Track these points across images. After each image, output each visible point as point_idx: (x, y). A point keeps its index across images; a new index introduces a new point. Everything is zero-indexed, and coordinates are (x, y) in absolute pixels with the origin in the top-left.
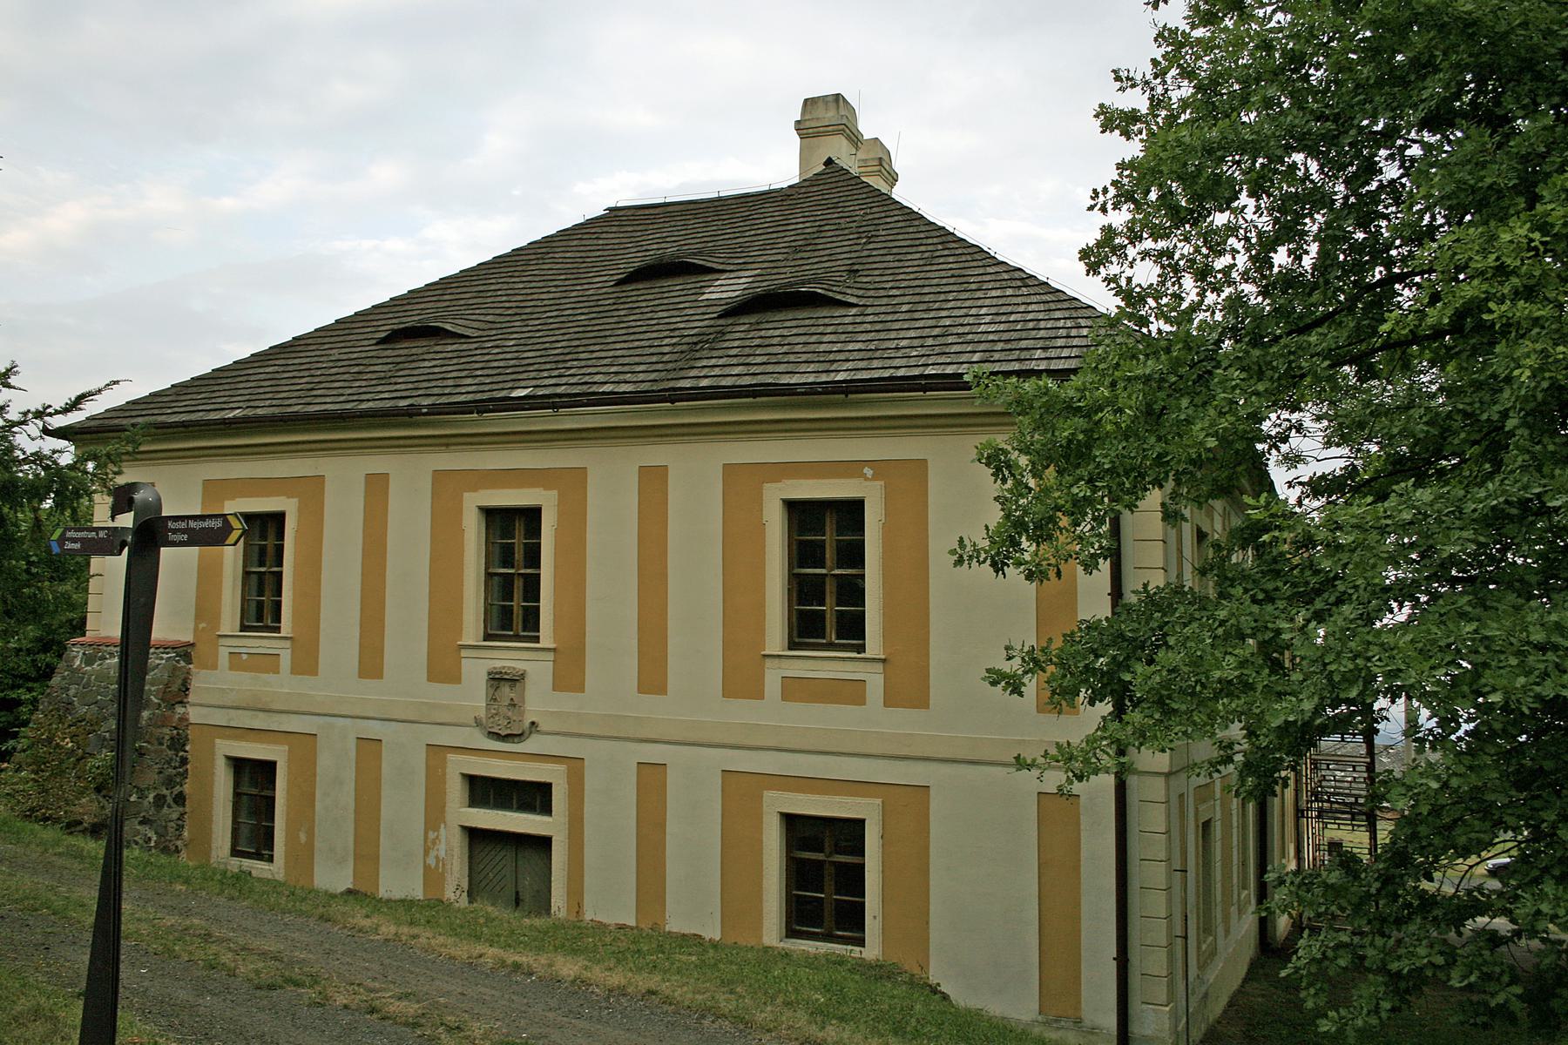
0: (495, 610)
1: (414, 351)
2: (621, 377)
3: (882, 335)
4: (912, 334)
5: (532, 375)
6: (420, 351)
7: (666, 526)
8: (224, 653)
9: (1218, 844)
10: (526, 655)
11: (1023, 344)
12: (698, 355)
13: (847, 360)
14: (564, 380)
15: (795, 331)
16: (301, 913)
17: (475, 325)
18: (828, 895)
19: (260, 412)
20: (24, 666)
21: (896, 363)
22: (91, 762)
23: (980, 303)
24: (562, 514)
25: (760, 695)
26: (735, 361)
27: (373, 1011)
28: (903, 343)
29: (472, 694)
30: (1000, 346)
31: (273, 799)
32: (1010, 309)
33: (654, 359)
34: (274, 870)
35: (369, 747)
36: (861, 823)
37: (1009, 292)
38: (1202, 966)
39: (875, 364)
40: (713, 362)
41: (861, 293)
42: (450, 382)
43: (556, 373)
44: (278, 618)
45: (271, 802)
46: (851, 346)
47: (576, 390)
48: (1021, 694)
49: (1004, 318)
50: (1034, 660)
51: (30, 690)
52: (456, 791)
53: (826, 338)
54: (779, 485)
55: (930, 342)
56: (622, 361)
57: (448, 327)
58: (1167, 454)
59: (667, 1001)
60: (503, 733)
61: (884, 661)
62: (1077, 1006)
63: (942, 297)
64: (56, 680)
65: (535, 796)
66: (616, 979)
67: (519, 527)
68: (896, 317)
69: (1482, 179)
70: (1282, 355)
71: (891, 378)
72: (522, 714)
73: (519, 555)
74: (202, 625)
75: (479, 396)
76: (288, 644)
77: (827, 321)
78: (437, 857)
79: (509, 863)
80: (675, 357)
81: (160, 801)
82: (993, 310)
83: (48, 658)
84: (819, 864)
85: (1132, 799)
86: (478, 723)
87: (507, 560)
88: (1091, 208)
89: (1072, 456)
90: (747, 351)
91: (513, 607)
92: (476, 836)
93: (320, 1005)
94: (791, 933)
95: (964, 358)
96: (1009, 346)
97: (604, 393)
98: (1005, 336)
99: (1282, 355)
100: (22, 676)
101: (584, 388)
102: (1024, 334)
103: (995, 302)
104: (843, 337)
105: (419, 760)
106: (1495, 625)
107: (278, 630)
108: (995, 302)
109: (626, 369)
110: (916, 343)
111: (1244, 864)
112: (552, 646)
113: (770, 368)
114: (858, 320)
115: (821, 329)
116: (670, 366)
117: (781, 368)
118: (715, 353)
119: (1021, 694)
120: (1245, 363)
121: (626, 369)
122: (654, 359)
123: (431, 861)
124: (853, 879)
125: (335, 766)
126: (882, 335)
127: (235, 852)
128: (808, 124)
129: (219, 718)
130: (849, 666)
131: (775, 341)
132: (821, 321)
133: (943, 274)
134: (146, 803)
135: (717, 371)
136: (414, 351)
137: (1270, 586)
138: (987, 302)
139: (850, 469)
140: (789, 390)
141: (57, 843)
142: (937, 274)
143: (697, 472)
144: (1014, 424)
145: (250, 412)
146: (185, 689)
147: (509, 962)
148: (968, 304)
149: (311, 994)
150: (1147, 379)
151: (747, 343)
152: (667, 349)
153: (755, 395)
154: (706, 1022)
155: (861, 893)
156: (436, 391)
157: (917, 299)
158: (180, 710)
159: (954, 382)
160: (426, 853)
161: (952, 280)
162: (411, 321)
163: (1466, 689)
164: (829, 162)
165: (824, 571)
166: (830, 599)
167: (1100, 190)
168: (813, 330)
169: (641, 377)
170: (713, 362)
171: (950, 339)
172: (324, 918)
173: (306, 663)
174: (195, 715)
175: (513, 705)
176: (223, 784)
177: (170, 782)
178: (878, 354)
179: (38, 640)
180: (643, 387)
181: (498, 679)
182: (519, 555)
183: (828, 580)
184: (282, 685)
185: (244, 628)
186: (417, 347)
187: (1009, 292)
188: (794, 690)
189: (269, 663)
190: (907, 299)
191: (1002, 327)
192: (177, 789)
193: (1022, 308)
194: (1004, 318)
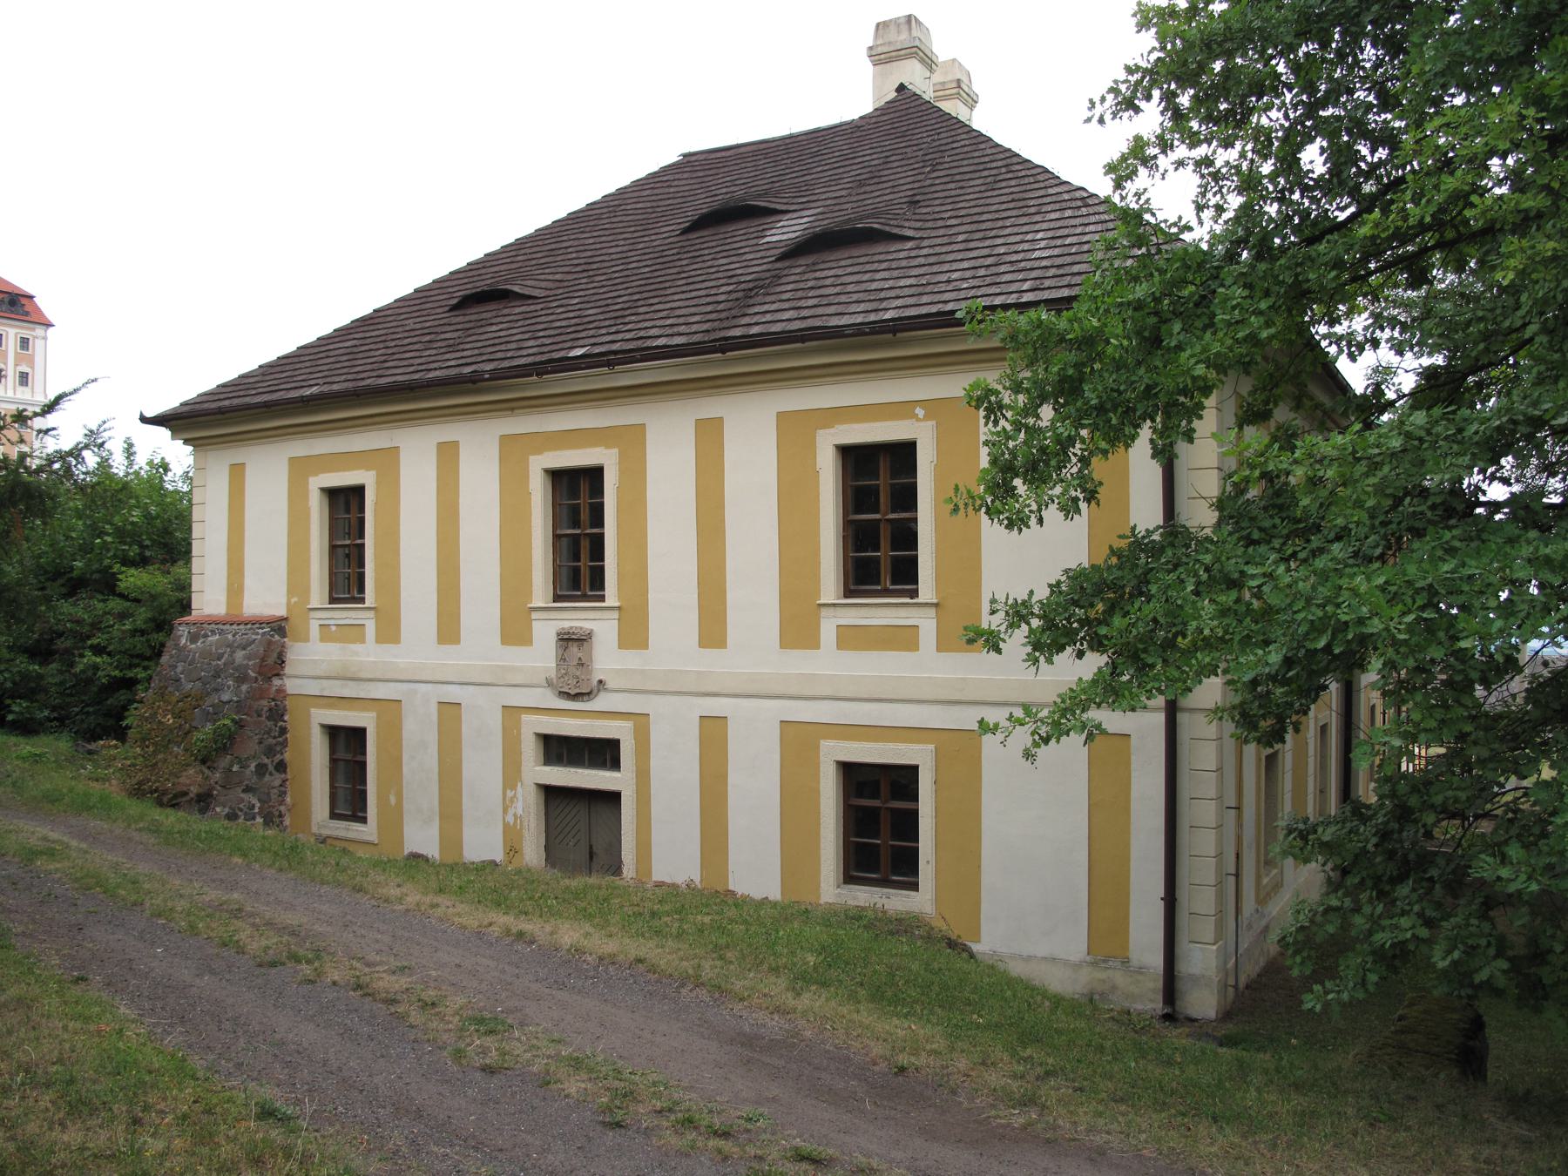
0: (564, 571)
1: (484, 315)
2: (675, 330)
3: (935, 269)
4: (966, 265)
5: (591, 333)
6: (489, 315)
7: (721, 483)
8: (314, 627)
9: (1288, 777)
10: (591, 615)
11: (1076, 269)
12: (751, 302)
13: (898, 297)
14: (620, 336)
15: (850, 270)
16: (339, 884)
17: (543, 284)
18: (883, 841)
19: (335, 387)
20: (139, 643)
21: (946, 296)
22: (197, 735)
23: (1037, 227)
24: (623, 472)
25: (815, 645)
26: (786, 305)
27: (359, 987)
28: (955, 276)
29: (541, 655)
30: (1052, 272)
31: (364, 763)
32: (1066, 232)
33: (709, 308)
34: (368, 831)
35: (450, 712)
36: (913, 770)
37: (1068, 213)
38: (1262, 900)
39: (925, 299)
40: (766, 308)
41: (918, 225)
42: (514, 346)
43: (614, 329)
44: (362, 589)
45: (363, 765)
46: (902, 283)
47: (631, 346)
48: (999, 651)
49: (1059, 242)
50: (1017, 613)
51: (145, 668)
52: (530, 750)
53: (879, 276)
54: (832, 431)
55: (982, 272)
56: (678, 312)
57: (516, 289)
58: (1157, 385)
59: (653, 969)
60: (573, 692)
61: (936, 605)
62: (1125, 947)
63: (1000, 224)
64: (164, 659)
65: (604, 752)
66: (610, 947)
67: (584, 487)
68: (950, 248)
69: (1479, 49)
70: (1289, 268)
71: (939, 313)
72: (590, 672)
73: (585, 516)
74: (294, 600)
75: (538, 359)
76: (371, 614)
77: (882, 257)
78: (515, 815)
79: (582, 820)
80: (729, 305)
81: (261, 770)
82: (1050, 234)
83: (161, 637)
84: (876, 810)
85: (1184, 735)
86: (549, 683)
87: (576, 523)
88: (1089, 120)
89: (1067, 389)
90: (800, 294)
91: (580, 566)
92: (551, 793)
93: (312, 982)
94: (849, 878)
95: (1014, 287)
96: (1061, 272)
97: (657, 347)
98: (1059, 261)
99: (1289, 268)
100: (138, 656)
101: (639, 344)
102: (1078, 258)
103: (1052, 225)
104: (895, 273)
105: (495, 721)
106: (1473, 563)
107: (362, 600)
108: (1052, 225)
109: (681, 320)
110: (968, 274)
111: (1323, 791)
112: (617, 604)
113: (820, 311)
114: (913, 254)
115: (875, 266)
116: (723, 315)
117: (832, 310)
118: (769, 299)
119: (999, 651)
120: (1249, 280)
121: (681, 320)
122: (709, 308)
123: (510, 819)
124: (908, 824)
125: (419, 731)
126: (935, 269)
127: (334, 815)
128: (880, 50)
129: (312, 688)
130: (903, 612)
131: (828, 282)
132: (876, 258)
133: (1004, 199)
134: (248, 772)
135: (768, 317)
136: (484, 315)
137: (1267, 524)
138: (1045, 226)
139: (901, 410)
140: (836, 333)
141: (141, 818)
142: (997, 200)
143: (752, 426)
144: (1004, 359)
145: (326, 389)
146: (281, 662)
147: (514, 931)
148: (1025, 229)
149: (307, 970)
150: (1138, 306)
151: (802, 285)
152: (722, 298)
153: (803, 339)
154: (684, 991)
155: (915, 837)
156: (499, 355)
157: (974, 227)
158: (276, 682)
159: (946, 320)
160: (505, 811)
161: (1011, 205)
162: (483, 285)
163: (1441, 634)
164: (901, 88)
165: (878, 516)
166: (885, 542)
167: (1097, 100)
168: (868, 267)
169: (694, 328)
170: (766, 308)
171: (1003, 268)
172: (359, 889)
173: (390, 631)
174: (292, 686)
175: (581, 664)
176: (318, 754)
177: (270, 751)
178: (929, 289)
179: (153, 620)
180: (696, 338)
181: (570, 640)
182: (585, 516)
183: (882, 526)
184: (368, 653)
185: (333, 600)
186: (487, 311)
187: (1068, 213)
188: (850, 638)
189: (354, 633)
190: (963, 228)
191: (1056, 252)
192: (278, 757)
193: (1079, 230)
194: (1059, 242)
